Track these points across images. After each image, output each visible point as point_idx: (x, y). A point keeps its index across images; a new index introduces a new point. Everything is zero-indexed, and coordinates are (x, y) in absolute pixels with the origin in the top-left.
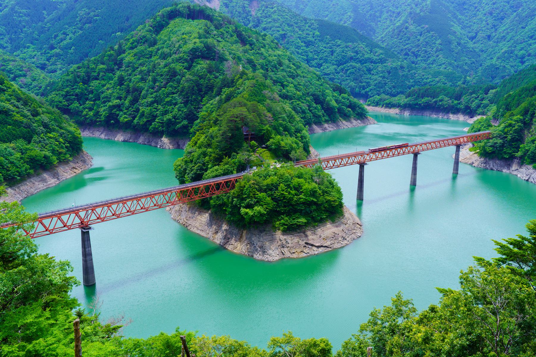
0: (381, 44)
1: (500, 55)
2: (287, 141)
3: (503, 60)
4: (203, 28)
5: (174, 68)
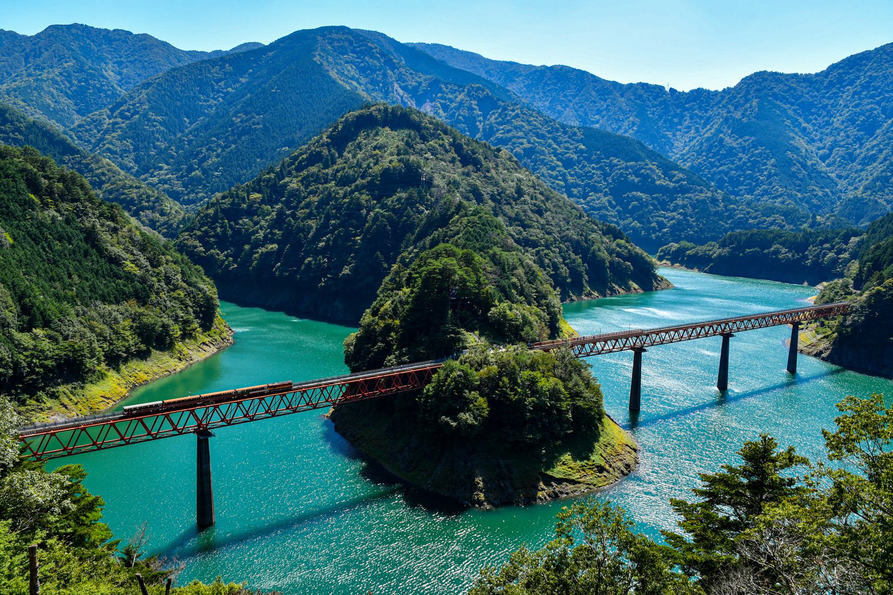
0: (682, 164)
1: (869, 183)
2: (516, 311)
3: (874, 191)
4: (405, 139)
5: (358, 199)
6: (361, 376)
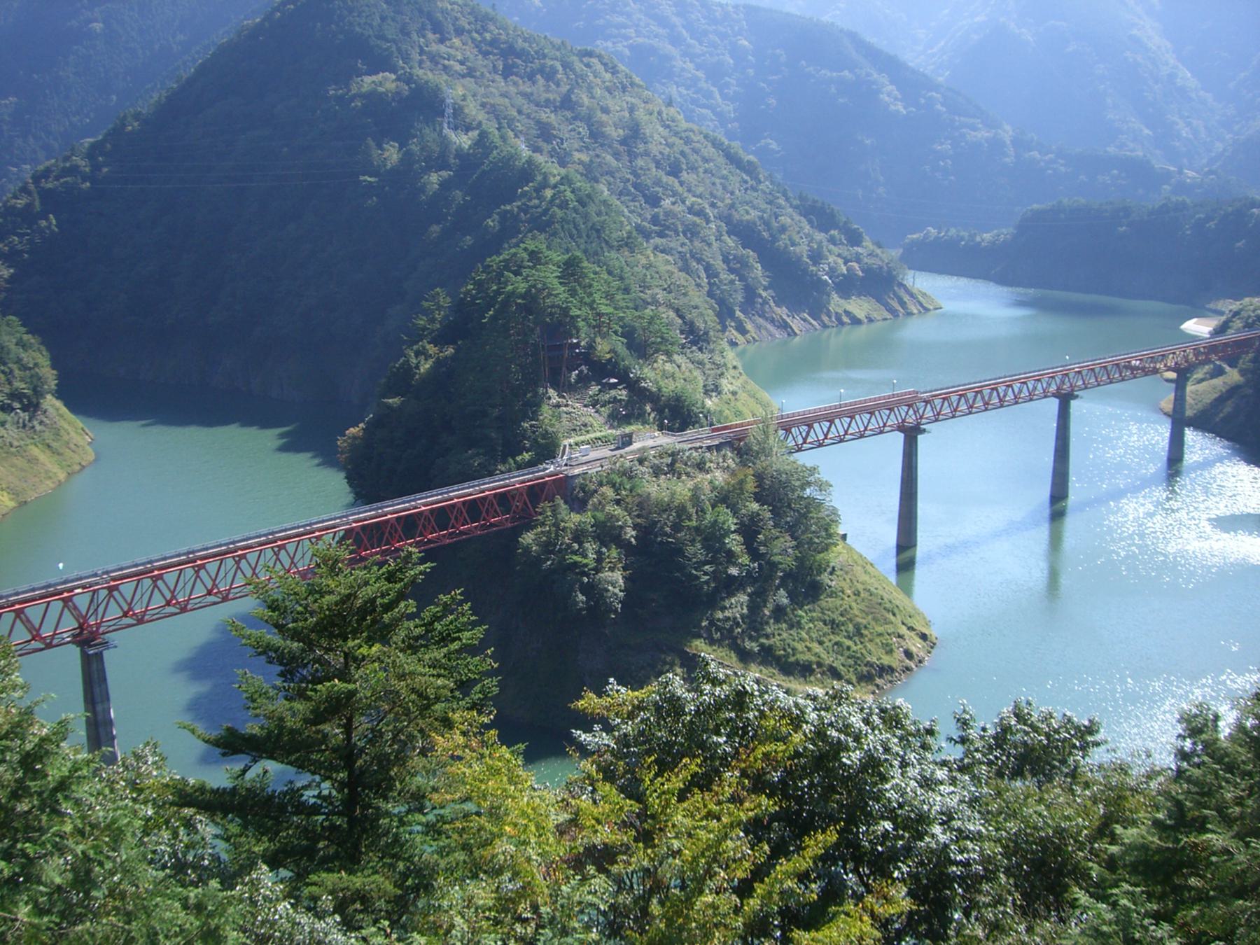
6: (393, 509)
